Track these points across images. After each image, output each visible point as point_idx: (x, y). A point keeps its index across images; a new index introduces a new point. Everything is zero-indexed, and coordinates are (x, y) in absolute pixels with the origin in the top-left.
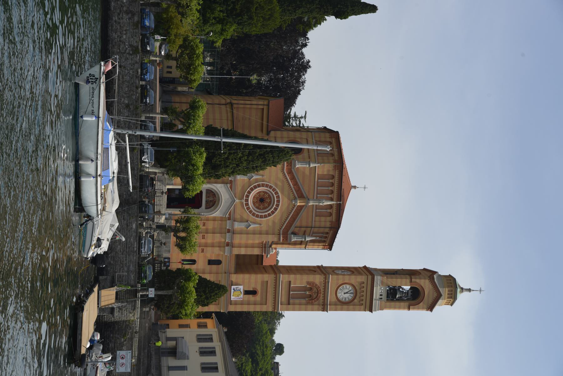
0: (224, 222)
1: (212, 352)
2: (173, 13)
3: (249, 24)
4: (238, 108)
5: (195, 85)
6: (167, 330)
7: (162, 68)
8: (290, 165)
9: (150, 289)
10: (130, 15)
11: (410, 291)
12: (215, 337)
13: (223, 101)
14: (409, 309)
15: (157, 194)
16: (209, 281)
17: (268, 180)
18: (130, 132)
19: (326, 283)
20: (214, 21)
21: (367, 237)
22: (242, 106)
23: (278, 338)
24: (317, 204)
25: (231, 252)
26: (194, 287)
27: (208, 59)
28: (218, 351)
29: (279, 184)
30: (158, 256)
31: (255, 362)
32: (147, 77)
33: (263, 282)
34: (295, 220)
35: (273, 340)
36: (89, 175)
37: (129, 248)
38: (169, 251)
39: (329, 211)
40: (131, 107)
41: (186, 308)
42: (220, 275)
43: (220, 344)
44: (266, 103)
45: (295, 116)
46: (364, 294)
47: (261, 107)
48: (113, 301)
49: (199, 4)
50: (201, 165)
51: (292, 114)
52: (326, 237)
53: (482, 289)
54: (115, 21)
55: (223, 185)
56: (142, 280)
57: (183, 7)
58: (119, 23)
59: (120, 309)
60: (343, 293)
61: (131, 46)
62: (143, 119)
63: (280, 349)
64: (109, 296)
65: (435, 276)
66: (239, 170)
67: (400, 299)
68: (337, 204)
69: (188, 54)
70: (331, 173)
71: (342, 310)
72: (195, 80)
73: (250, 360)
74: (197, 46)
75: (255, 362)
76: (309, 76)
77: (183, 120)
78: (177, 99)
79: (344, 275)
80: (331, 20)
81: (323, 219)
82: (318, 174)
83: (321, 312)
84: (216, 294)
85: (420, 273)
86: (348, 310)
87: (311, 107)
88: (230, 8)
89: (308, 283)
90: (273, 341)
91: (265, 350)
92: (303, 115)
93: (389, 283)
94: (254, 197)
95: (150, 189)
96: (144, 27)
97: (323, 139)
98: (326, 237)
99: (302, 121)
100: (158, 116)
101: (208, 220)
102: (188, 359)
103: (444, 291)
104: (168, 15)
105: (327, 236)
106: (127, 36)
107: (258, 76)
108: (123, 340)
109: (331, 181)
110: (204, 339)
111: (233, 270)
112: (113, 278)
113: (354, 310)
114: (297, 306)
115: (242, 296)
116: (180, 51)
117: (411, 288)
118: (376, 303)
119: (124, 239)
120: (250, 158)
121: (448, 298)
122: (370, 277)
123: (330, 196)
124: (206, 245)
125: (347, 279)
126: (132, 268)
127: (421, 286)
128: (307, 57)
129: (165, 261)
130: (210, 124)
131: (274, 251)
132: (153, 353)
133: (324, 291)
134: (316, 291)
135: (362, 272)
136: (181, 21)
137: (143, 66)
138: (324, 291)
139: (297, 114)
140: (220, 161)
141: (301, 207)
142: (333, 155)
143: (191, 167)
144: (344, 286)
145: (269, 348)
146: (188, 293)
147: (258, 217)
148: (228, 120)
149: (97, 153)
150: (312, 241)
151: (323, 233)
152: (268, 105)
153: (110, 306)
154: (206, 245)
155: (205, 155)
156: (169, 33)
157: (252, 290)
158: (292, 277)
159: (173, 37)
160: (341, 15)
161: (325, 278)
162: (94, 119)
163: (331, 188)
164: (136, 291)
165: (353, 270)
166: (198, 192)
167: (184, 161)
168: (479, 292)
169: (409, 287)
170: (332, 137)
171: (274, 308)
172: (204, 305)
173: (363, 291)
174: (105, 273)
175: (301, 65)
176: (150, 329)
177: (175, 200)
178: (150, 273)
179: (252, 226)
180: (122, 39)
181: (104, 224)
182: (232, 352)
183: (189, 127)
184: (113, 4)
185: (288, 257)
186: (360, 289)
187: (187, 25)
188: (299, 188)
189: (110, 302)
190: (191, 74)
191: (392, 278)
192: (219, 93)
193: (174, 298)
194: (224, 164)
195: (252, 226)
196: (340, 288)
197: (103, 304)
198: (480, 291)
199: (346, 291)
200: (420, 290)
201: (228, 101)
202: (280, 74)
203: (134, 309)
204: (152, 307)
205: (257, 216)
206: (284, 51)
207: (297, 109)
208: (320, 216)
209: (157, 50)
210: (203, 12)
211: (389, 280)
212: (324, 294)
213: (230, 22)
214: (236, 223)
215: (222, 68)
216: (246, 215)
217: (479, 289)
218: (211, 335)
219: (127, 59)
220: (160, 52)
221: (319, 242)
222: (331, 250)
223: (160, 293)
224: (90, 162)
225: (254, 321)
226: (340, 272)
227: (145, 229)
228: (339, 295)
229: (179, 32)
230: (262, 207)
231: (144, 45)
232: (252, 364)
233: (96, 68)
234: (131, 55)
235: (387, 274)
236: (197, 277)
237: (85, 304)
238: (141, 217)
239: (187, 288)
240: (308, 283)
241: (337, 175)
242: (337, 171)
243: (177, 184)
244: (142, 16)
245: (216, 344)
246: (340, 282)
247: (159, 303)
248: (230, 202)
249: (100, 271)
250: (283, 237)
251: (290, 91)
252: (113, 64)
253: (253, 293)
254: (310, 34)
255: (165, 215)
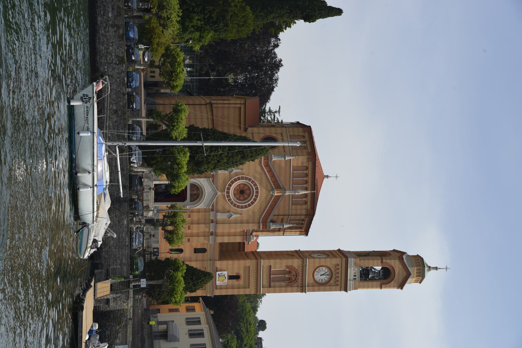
0: (207, 213)
1: (200, 334)
2: (155, 24)
3: (225, 30)
4: (217, 107)
5: (177, 90)
6: (159, 315)
7: (146, 74)
8: (267, 159)
9: (142, 280)
10: (115, 28)
11: (381, 271)
12: (203, 320)
13: (203, 102)
14: (381, 288)
15: (145, 190)
16: (196, 269)
17: (247, 174)
18: (120, 144)
19: (303, 266)
20: (192, 29)
21: (342, 222)
22: (221, 105)
23: (260, 315)
24: (293, 193)
25: (215, 240)
26: (182, 276)
27: (187, 62)
28: (206, 333)
29: (258, 176)
30: (148, 247)
31: (240, 338)
32: (134, 84)
33: (245, 267)
34: (273, 209)
35: (256, 317)
36: (86, 186)
37: (121, 242)
38: (158, 242)
39: (304, 199)
40: (119, 113)
41: (176, 296)
42: (205, 262)
43: (207, 326)
44: (243, 102)
45: (270, 111)
46: (339, 275)
47: (239, 106)
48: (109, 292)
49: (178, 16)
50: (185, 164)
51: (267, 109)
52: (302, 224)
53: (448, 267)
54: (102, 35)
55: (205, 179)
56: (134, 272)
57: (164, 18)
58: (106, 36)
59: (115, 299)
60: (319, 275)
61: (117, 56)
62: (130, 122)
63: (262, 325)
64: (104, 288)
65: (404, 257)
66: (220, 165)
67: (373, 279)
68: (312, 193)
69: (169, 63)
70: (305, 164)
71: (319, 291)
72: (177, 86)
73: (236, 337)
74: (178, 55)
75: (240, 338)
76: (281, 74)
77: (167, 123)
78: (160, 101)
79: (320, 258)
80: (300, 23)
81: (299, 207)
82: (293, 166)
83: (300, 294)
84: (203, 281)
85: (390, 254)
86: (325, 290)
87: (285, 103)
88: (207, 17)
89: (287, 267)
90: (256, 318)
91: (249, 326)
92: (277, 110)
93: (362, 265)
94: (235, 189)
95: (139, 187)
96: (128, 39)
97: (296, 134)
98: (302, 224)
99: (277, 115)
100: (144, 121)
101: (192, 211)
102: (178, 341)
103: (413, 270)
104: (150, 25)
105: (303, 222)
106: (112, 47)
107: (235, 76)
108: (118, 327)
109: (305, 172)
110: (192, 322)
111: (217, 257)
112: (108, 270)
113: (330, 290)
114: (278, 289)
115: (226, 281)
116: (162, 59)
117: (382, 268)
118: (350, 283)
119: (115, 236)
120: (230, 155)
121: (417, 276)
122: (344, 259)
123: (305, 186)
124: (192, 235)
125: (323, 262)
126: (124, 261)
127: (392, 267)
128: (279, 57)
129: (154, 252)
130: (192, 124)
131: (255, 238)
132: (146, 337)
133: (303, 274)
134: (293, 274)
135: (336, 254)
136: (163, 32)
137: (129, 75)
138: (303, 274)
139: (271, 109)
140: (202, 158)
141: (278, 197)
142: (306, 148)
143: (176, 166)
144: (321, 268)
145: (252, 325)
146: (177, 282)
147: (239, 208)
148: (208, 119)
149: (93, 165)
150: (289, 228)
151: (299, 220)
152: (245, 104)
153: (106, 297)
154: (192, 235)
155: (188, 154)
156: (151, 42)
157: (235, 275)
158: (272, 262)
159: (155, 46)
160: (309, 18)
161: (303, 262)
162: (89, 134)
163: (305, 179)
164: (129, 282)
165: (328, 253)
166: (184, 188)
167: (170, 161)
168: (445, 270)
169: (381, 267)
170: (303, 132)
171: (257, 291)
172: (192, 291)
173: (338, 273)
174: (100, 266)
175: (273, 64)
176: (142, 315)
177: (162, 194)
178: (141, 264)
179: (234, 216)
180: (109, 50)
181: (100, 226)
182: (218, 331)
183: (173, 129)
184: (99, 19)
185: (267, 243)
186: (335, 271)
187: (169, 34)
188: (276, 180)
189: (105, 294)
190: (174, 80)
191: (364, 260)
192: (199, 94)
193: (164, 287)
194: (206, 160)
195: (234, 216)
196: (317, 270)
197: (98, 296)
198: (446, 268)
199: (323, 273)
200: (390, 269)
201: (208, 101)
202: (255, 73)
203: (128, 299)
204: (144, 295)
205: (238, 207)
206: (257, 52)
207: (271, 105)
208: (296, 205)
209: (141, 57)
210: (182, 22)
211: (362, 261)
212: (302, 276)
213: (208, 30)
214: (219, 214)
215: (201, 70)
216: (228, 206)
217: (445, 267)
218: (202, 330)
219: (114, 69)
220: (144, 59)
221: (296, 228)
222: (307, 235)
223: (151, 283)
224: (88, 174)
225: (238, 302)
226: (316, 256)
227: (135, 224)
228: (316, 277)
229: (160, 41)
230: (242, 198)
231: (129, 55)
232: (237, 341)
233: (90, 88)
234: (118, 65)
235: (360, 256)
236: (185, 267)
237: (83, 303)
238: (131, 214)
239: (176, 278)
240: (287, 267)
241: (310, 166)
242: (310, 163)
243: (163, 180)
244: (126, 29)
245: (204, 326)
246: (317, 265)
247: (150, 291)
248: (212, 195)
249: (97, 266)
250: (263, 225)
251: (264, 88)
252: (103, 83)
253: (237, 277)
254: (281, 35)
255: (154, 209)
